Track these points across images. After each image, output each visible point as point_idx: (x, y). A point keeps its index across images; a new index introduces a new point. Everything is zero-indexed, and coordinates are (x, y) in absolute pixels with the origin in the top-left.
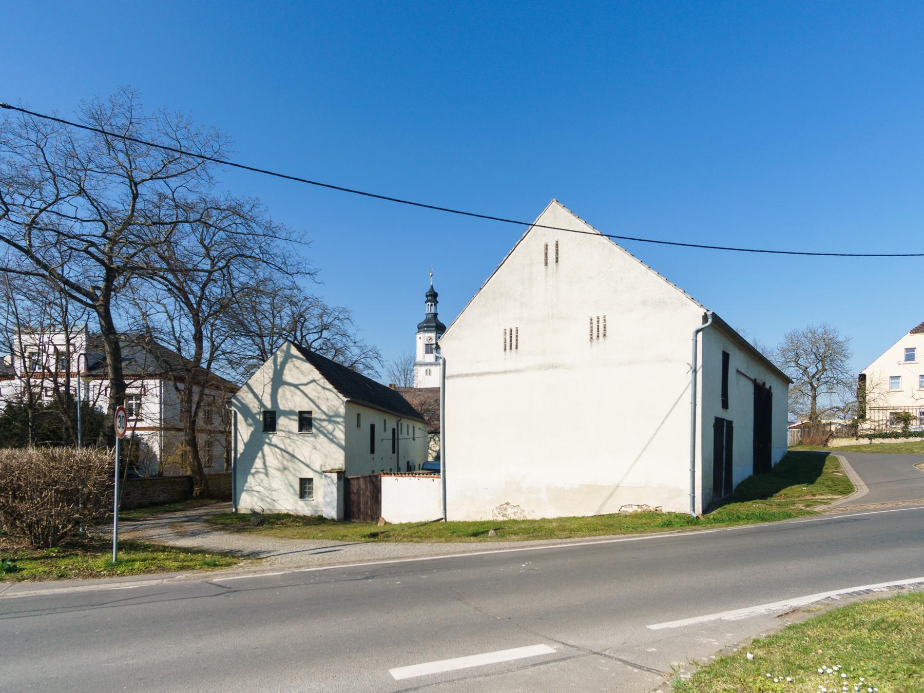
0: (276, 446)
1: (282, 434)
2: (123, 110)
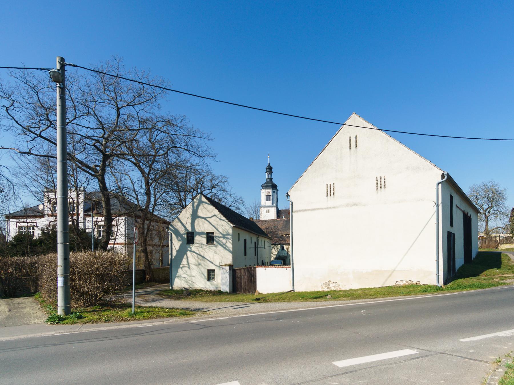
0: (194, 252)
1: (198, 245)
2: (114, 68)
